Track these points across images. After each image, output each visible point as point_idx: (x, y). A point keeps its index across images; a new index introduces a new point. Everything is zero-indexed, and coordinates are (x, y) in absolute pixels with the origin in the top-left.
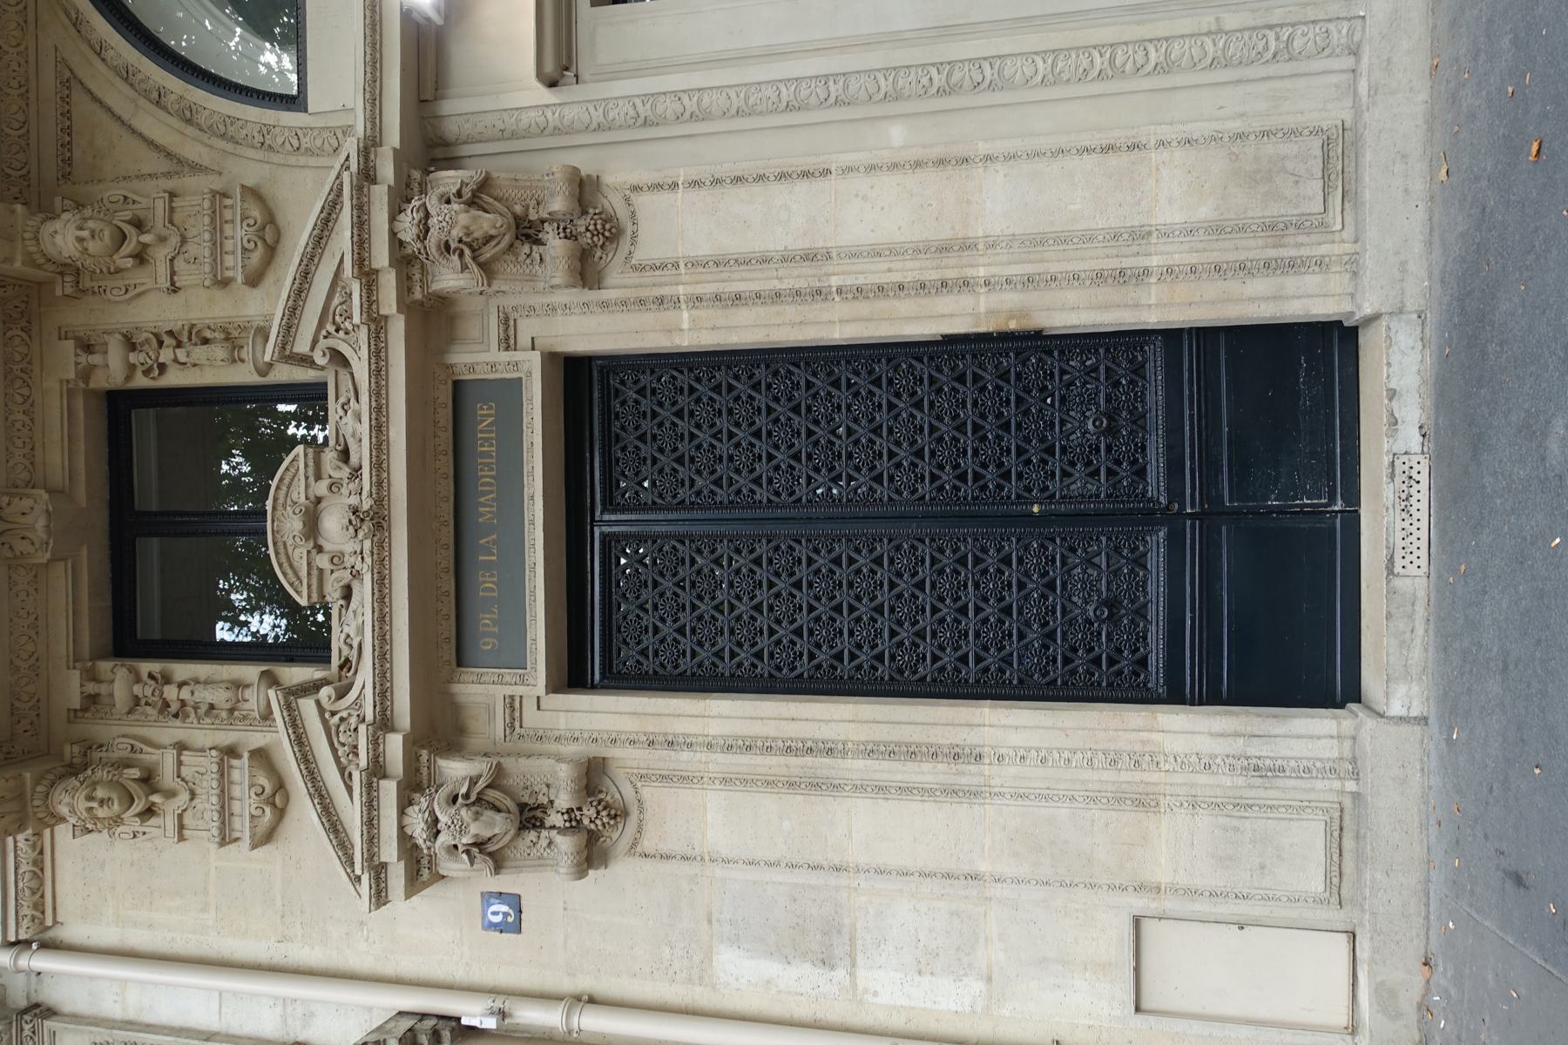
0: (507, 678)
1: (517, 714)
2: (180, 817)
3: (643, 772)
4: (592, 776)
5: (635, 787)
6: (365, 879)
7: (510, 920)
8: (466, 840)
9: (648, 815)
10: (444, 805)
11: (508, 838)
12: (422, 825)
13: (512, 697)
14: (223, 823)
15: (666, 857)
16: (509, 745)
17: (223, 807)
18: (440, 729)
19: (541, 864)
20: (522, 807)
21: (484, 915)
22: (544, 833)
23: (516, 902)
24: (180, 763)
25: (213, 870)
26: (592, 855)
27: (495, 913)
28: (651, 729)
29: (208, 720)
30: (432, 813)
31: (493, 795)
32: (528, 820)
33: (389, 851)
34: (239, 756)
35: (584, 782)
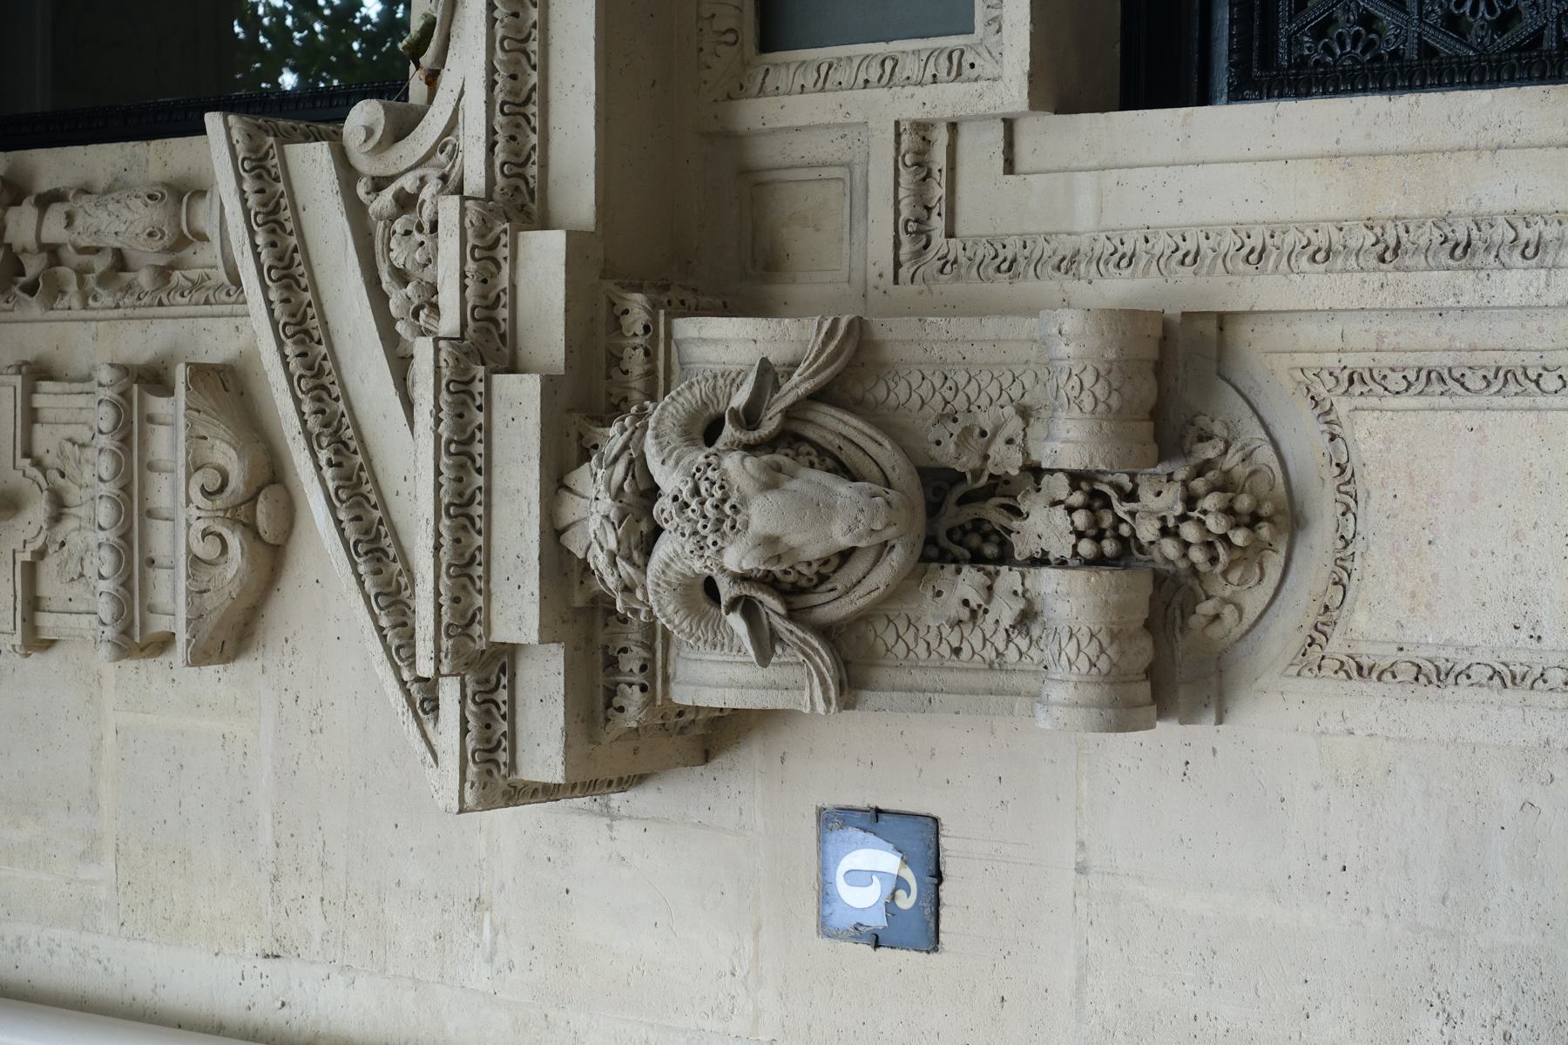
0: (910, 67)
1: (939, 192)
2: (31, 571)
3: (1354, 361)
4: (1176, 374)
5: (1327, 415)
6: (449, 692)
7: (905, 902)
8: (738, 556)
9: (1371, 515)
10: (673, 437)
11: (882, 576)
12: (606, 504)
13: (923, 129)
14: (126, 584)
15: (1435, 675)
16: (906, 289)
17: (125, 537)
18: (692, 225)
19: (999, 687)
20: (938, 484)
21: (825, 894)
22: (1009, 578)
23: (922, 840)
24: (31, 416)
25: (110, 738)
26: (1169, 663)
27: (858, 878)
28: (1392, 205)
29: (106, 298)
30: (638, 466)
31: (833, 424)
32: (958, 534)
33: (516, 611)
34: (167, 390)
35: (1147, 390)
